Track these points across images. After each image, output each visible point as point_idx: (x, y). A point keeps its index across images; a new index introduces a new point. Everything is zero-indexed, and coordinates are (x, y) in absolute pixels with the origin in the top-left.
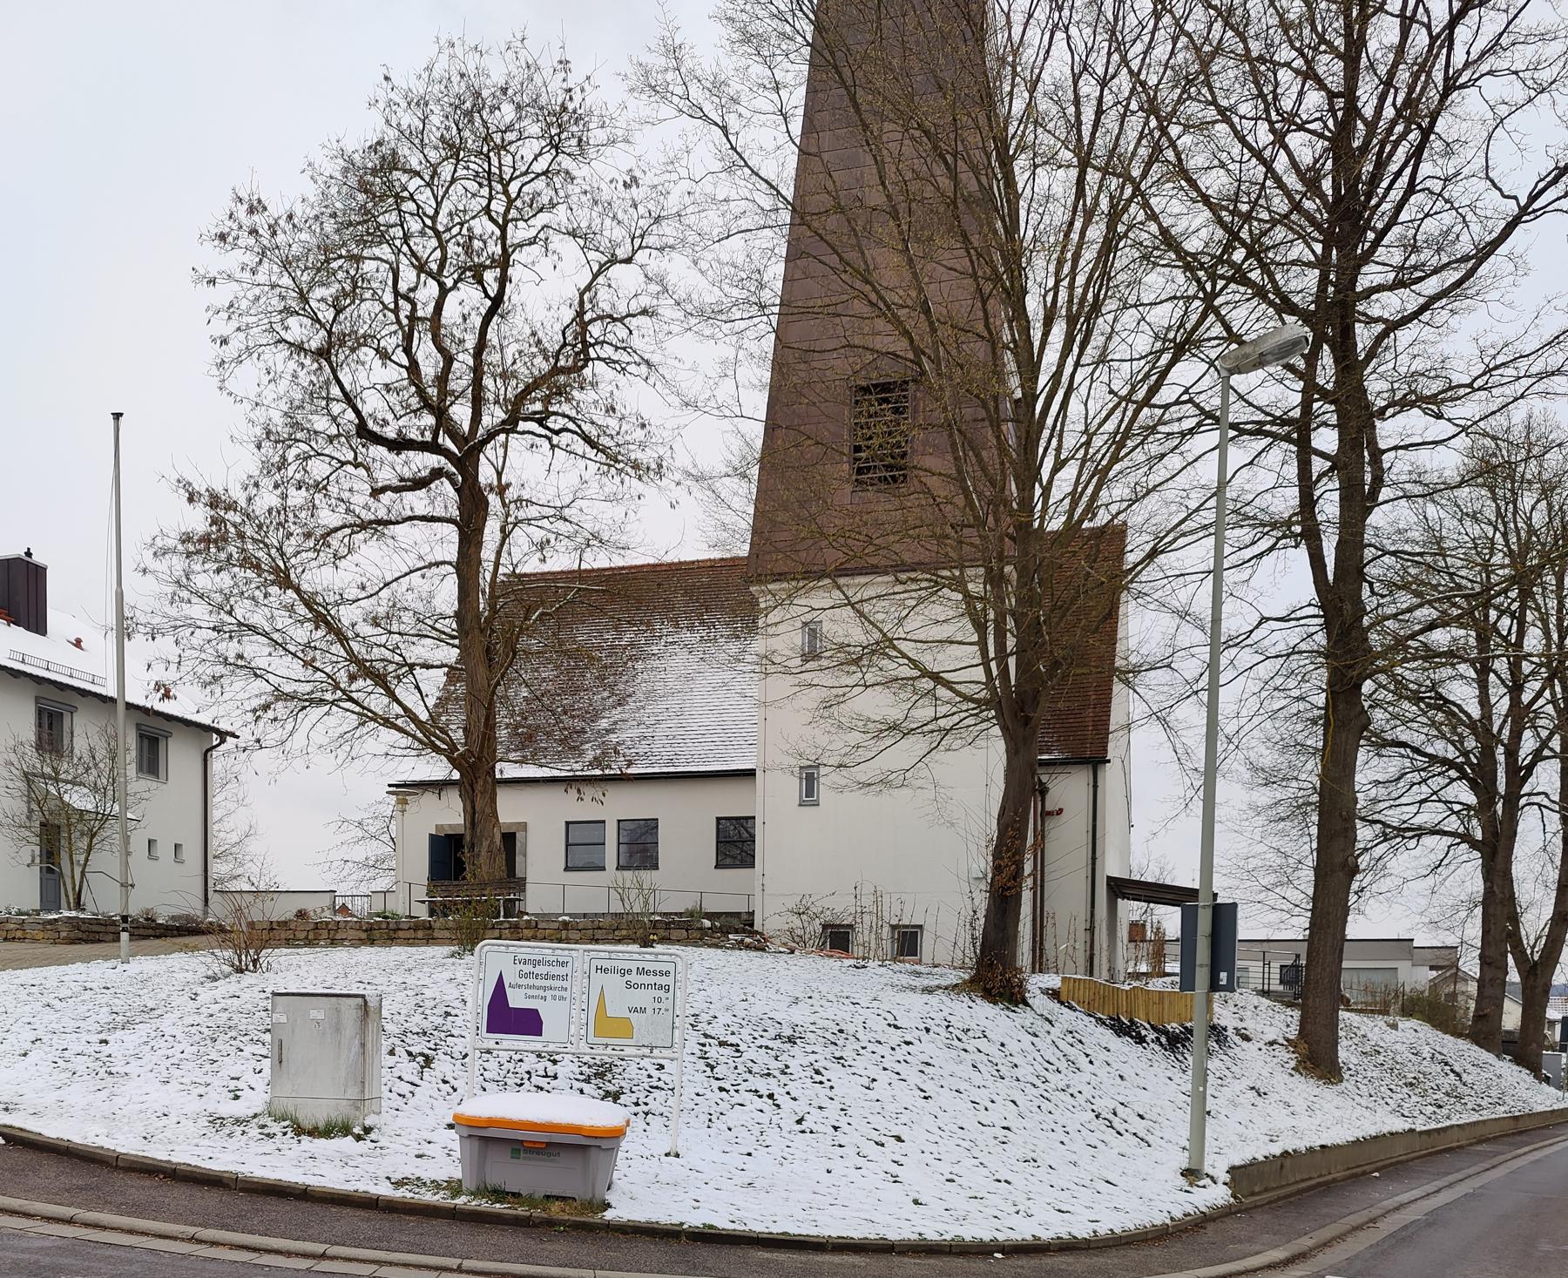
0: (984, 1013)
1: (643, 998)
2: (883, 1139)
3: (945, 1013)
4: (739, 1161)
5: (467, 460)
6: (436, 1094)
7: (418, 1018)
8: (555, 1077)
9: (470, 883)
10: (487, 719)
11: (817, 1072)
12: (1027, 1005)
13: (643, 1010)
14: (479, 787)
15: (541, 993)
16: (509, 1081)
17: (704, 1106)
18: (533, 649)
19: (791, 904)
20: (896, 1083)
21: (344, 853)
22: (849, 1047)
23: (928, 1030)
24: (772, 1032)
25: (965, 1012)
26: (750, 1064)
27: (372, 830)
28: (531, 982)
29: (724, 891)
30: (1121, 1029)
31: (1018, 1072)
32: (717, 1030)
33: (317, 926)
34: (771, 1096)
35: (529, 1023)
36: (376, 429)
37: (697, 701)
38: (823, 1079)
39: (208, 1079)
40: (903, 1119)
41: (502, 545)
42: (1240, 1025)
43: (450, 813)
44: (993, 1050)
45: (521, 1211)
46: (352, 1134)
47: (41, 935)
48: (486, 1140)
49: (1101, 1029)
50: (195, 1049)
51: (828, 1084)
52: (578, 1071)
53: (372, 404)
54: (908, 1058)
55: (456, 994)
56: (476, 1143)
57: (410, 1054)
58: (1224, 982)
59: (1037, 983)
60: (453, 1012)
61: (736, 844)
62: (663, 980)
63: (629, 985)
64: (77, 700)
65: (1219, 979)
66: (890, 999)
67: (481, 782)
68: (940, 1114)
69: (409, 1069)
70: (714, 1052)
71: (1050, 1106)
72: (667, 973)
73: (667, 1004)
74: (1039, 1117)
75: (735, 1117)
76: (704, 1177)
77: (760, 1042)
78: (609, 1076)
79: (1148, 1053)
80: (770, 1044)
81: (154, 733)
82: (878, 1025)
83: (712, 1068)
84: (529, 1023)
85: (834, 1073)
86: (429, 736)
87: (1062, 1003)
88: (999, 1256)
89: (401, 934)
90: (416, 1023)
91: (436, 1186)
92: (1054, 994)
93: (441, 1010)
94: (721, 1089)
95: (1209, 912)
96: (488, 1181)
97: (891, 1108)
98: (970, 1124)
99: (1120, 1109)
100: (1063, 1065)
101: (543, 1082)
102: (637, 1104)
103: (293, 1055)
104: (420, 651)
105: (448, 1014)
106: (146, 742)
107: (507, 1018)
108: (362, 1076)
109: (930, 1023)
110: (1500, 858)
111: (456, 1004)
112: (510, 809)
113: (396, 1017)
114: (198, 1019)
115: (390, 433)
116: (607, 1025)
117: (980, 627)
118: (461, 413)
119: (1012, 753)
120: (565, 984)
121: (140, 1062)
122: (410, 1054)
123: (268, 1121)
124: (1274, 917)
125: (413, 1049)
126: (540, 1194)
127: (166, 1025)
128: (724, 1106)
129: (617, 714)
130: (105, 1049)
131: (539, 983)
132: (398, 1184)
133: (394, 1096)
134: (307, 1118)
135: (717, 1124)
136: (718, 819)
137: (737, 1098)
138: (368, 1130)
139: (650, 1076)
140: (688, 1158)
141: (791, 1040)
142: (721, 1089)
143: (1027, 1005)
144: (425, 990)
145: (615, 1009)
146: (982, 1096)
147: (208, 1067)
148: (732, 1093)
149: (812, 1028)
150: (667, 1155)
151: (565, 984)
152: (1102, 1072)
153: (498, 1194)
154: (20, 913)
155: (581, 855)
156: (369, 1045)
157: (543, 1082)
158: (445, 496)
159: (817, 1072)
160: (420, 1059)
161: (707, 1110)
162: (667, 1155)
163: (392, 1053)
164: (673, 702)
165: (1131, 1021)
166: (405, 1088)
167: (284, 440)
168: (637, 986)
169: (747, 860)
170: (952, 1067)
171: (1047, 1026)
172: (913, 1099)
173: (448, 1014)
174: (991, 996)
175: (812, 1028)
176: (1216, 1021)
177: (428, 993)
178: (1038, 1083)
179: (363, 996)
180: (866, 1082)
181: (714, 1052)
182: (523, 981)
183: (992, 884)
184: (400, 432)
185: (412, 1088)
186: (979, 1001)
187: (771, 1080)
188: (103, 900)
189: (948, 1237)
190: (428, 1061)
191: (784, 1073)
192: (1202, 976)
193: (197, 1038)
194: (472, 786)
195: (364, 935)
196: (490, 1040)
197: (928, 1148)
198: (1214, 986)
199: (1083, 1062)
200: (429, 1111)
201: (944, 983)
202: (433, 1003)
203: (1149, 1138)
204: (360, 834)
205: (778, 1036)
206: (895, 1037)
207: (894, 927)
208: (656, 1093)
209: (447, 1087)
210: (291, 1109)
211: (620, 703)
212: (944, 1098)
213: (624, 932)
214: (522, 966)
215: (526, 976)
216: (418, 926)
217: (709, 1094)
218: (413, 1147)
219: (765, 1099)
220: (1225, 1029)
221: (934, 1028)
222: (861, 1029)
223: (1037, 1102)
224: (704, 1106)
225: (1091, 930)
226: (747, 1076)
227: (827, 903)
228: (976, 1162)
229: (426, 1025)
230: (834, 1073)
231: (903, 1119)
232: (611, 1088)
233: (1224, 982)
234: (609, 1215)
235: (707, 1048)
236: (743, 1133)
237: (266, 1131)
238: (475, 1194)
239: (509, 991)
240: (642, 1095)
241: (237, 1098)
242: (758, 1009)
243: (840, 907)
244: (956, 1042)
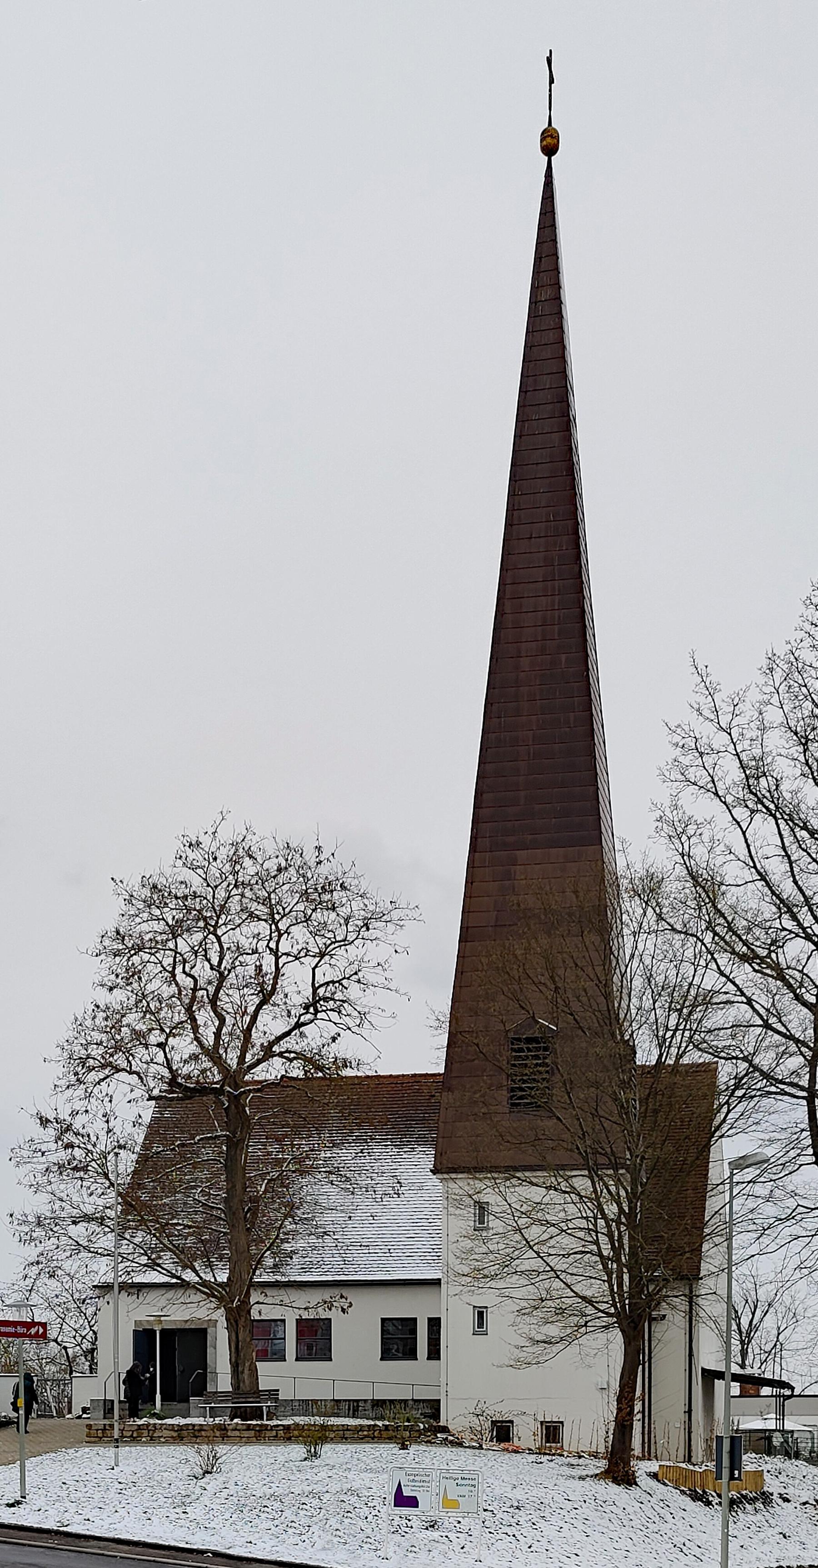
0: (614, 1490)
1: (464, 1490)
3: (593, 1492)
11: (534, 1524)
12: (637, 1485)
22: (547, 1511)
23: (585, 1502)
25: (604, 1491)
28: (413, 1484)
30: (695, 1497)
31: (633, 1523)
34: (514, 1536)
35: (412, 1502)
42: (783, 1491)
44: (619, 1511)
49: (683, 1497)
58: (736, 1476)
59: (643, 1468)
62: (473, 1482)
67: (243, 1319)
71: (650, 1541)
74: (644, 1546)
77: (504, 1509)
78: (436, 1527)
79: (712, 1512)
80: (508, 1510)
82: (559, 1499)
84: (412, 1502)
85: (541, 1524)
87: (659, 1481)
92: (654, 1476)
99: (687, 1543)
100: (657, 1519)
117: (609, 1274)
119: (627, 1344)
131: (417, 1484)
135: (492, 1548)
136: (384, 1320)
137: (498, 1537)
143: (637, 1485)
152: (680, 1524)
159: (534, 1524)
165: (704, 1491)
171: (649, 1497)
174: (617, 1481)
176: (765, 1489)
180: (558, 1529)
183: (616, 1418)
186: (610, 1484)
192: (726, 1473)
194: (236, 1322)
195: (175, 1434)
198: (732, 1478)
199: (669, 1517)
201: (591, 1473)
203: (702, 1558)
206: (569, 1505)
207: (542, 1423)
213: (365, 1433)
220: (772, 1494)
221: (588, 1501)
225: (689, 1412)
230: (541, 1524)
233: (736, 1476)
242: (497, 1492)
244: (600, 1508)
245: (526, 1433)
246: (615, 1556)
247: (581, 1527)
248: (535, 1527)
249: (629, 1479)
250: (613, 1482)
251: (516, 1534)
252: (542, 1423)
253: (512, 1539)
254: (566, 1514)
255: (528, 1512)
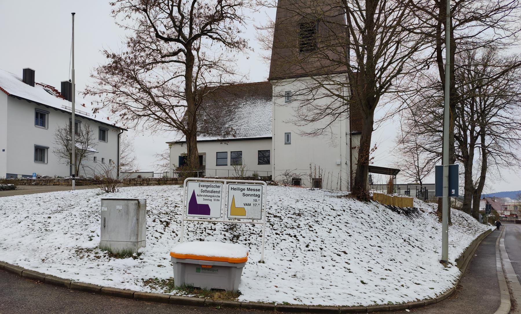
0: (358, 205)
2: (340, 253)
4: (287, 264)
5: (188, 43)
6: (170, 237)
7: (165, 208)
8: (215, 230)
9: (190, 166)
10: (194, 119)
11: (310, 227)
13: (250, 205)
14: (191, 140)
15: (210, 198)
16: (198, 232)
17: (271, 241)
18: (207, 107)
19: (283, 172)
20: (338, 230)
21: (158, 163)
23: (344, 211)
24: (292, 212)
26: (286, 224)
27: (165, 156)
28: (206, 194)
29: (263, 170)
32: (272, 211)
33: (143, 180)
34: (295, 236)
35: (205, 210)
36: (161, 35)
37: (253, 118)
38: (313, 229)
39: (82, 232)
40: (345, 244)
41: (198, 71)
43: (184, 150)
44: (366, 217)
45: (200, 299)
46: (132, 256)
47: (64, 183)
48: (185, 265)
50: (81, 220)
51: (315, 231)
52: (223, 227)
53: (161, 28)
54: (340, 221)
55: (180, 199)
56: (180, 266)
57: (161, 221)
60: (178, 206)
61: (264, 158)
63: (244, 195)
64: (81, 119)
65: (451, 192)
66: (329, 200)
68: (356, 242)
69: (160, 227)
70: (272, 219)
72: (259, 190)
73: (259, 202)
75: (283, 245)
76: (277, 272)
77: (288, 215)
78: (235, 229)
80: (292, 216)
81: (104, 129)
82: (328, 209)
83: (272, 225)
84: (205, 210)
85: (316, 227)
86: (179, 126)
88: (408, 310)
89: (168, 182)
90: (165, 209)
91: (163, 283)
93: (174, 205)
94: (277, 234)
95: (448, 168)
96: (186, 282)
97: (339, 240)
98: (368, 246)
101: (210, 232)
102: (246, 240)
103: (110, 224)
104: (174, 101)
105: (176, 206)
106: (102, 132)
107: (197, 208)
108: (137, 231)
109: (344, 208)
110: (469, 162)
111: (180, 203)
112: (201, 149)
113: (157, 208)
114: (86, 209)
115: (165, 36)
116: (236, 211)
118: (186, 31)
120: (219, 195)
121: (59, 225)
122: (161, 221)
123: (99, 250)
124: (404, 178)
125: (163, 220)
126: (209, 288)
127: (74, 212)
128: (278, 241)
129: (230, 123)
130: (49, 220)
132: (146, 282)
133: (153, 238)
134: (114, 250)
135: (277, 248)
138: (139, 254)
139: (250, 229)
140: (269, 264)
141: (299, 215)
142: (277, 234)
144: (169, 198)
145: (239, 204)
146: (368, 234)
147: (84, 227)
148: (281, 235)
149: (306, 210)
150: (259, 262)
151: (219, 195)
153: (190, 289)
154: (59, 177)
155: (221, 161)
156: (140, 220)
157: (210, 232)
158: (182, 56)
159: (310, 227)
160: (165, 223)
161: (272, 242)
162: (259, 262)
163: (154, 221)
164: (246, 120)
166: (158, 235)
167: (136, 43)
168: (248, 195)
169: (268, 162)
170: (354, 224)
172: (345, 236)
173: (176, 206)
175: (306, 210)
177: (170, 199)
178: (383, 229)
179: (138, 200)
180: (328, 230)
181: (272, 219)
182: (203, 194)
184: (168, 36)
185: (160, 235)
187: (294, 230)
188: (85, 173)
189: (386, 302)
190: (168, 224)
191: (298, 227)
193: (83, 216)
195: (157, 182)
196: (191, 217)
197: (357, 256)
200: (166, 244)
202: (171, 202)
204: (162, 158)
205: (294, 214)
206: (334, 213)
207: (313, 179)
208: (253, 236)
209: (174, 234)
210: (109, 246)
211: (231, 120)
212: (356, 235)
214: (202, 188)
215: (204, 191)
216: (176, 180)
217: (272, 236)
218: (152, 268)
219: (293, 237)
221: (346, 210)
222: (322, 210)
223: (385, 236)
224: (271, 241)
226: (285, 228)
227: (294, 172)
228: (375, 262)
229: (168, 210)
230: (316, 227)
231: (345, 244)
232: (236, 234)
233: (454, 193)
234: (241, 299)
235: (270, 218)
236: (287, 251)
237: (97, 255)
238: (181, 289)
239: (197, 198)
240: (247, 236)
241: (91, 240)
242: (285, 204)
243: (298, 173)
244: (354, 215)
245: (306, 181)
246: (373, 251)
247: (344, 229)
248: (311, 229)
249: (366, 198)
250: (357, 199)
251: (298, 235)
252: (313, 179)
253: (293, 239)
254: (333, 219)
255: (306, 218)
